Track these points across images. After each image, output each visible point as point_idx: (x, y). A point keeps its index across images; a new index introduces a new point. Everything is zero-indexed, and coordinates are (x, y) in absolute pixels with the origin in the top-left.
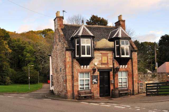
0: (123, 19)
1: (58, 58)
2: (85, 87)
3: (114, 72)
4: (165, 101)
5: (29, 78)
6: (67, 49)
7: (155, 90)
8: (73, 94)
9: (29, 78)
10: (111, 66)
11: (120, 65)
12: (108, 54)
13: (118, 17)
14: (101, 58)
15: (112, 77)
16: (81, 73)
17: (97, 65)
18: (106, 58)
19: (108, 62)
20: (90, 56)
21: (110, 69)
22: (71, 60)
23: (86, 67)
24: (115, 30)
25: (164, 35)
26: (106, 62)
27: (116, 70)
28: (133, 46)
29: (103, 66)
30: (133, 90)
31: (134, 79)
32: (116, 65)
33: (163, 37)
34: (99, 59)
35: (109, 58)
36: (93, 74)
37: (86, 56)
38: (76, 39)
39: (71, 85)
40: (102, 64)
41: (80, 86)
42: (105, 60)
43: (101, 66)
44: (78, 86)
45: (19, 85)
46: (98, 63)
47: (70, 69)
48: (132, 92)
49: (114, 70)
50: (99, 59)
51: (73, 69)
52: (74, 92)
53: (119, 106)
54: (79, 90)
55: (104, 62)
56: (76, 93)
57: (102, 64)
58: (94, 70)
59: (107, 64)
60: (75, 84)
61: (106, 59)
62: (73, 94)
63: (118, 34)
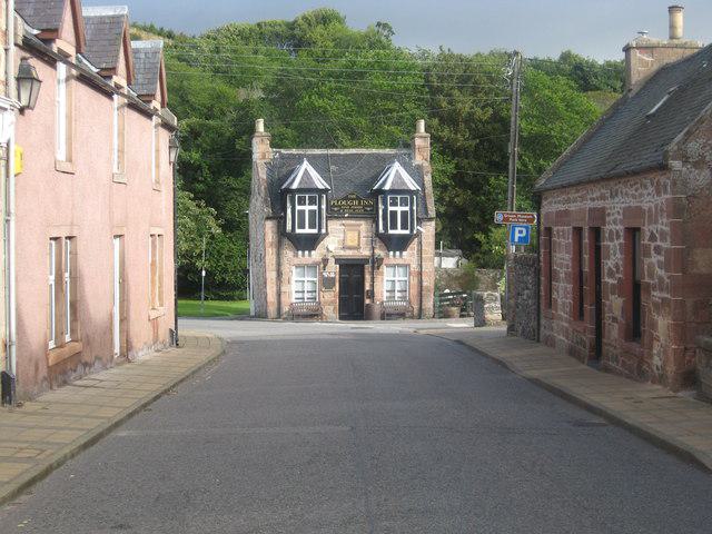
2: (306, 295)
3: (373, 268)
5: (204, 273)
6: (586, 352)
8: (279, 309)
9: (204, 273)
14: (342, 235)
15: (368, 277)
16: (297, 266)
20: (315, 231)
21: (366, 261)
22: (275, 240)
23: (310, 255)
24: (294, 151)
26: (355, 244)
27: (376, 263)
28: (642, 292)
29: (349, 254)
30: (421, 309)
32: (379, 252)
35: (363, 234)
37: (307, 230)
39: (275, 289)
41: (294, 295)
42: (352, 239)
43: (342, 253)
44: (290, 293)
47: (274, 257)
48: (416, 312)
49: (373, 263)
52: (283, 305)
53: (338, 327)
54: (294, 301)
55: (349, 243)
56: (286, 309)
58: (325, 261)
59: (358, 248)
60: (283, 289)
61: (356, 238)
62: (279, 309)
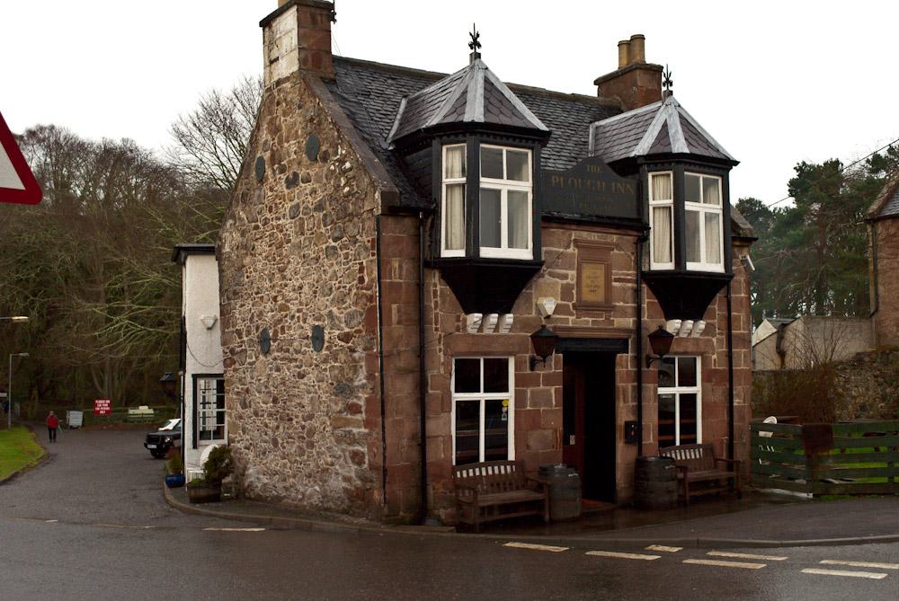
0: (651, 57)
1: (294, 262)
4: (878, 541)
7: (823, 562)
10: (629, 322)
11: (669, 316)
12: (609, 248)
13: (620, 44)
14: (572, 273)
17: (555, 312)
18: (600, 271)
19: (608, 299)
25: (818, 160)
26: (599, 297)
31: (736, 402)
33: (622, 176)
34: (566, 277)
36: (532, 368)
38: (442, 145)
40: (583, 308)
45: (685, 239)
46: (560, 302)
49: (639, 349)
50: (566, 277)
51: (422, 332)
55: (588, 297)
57: (583, 308)
59: (607, 307)
61: (601, 281)
63: (462, 101)
